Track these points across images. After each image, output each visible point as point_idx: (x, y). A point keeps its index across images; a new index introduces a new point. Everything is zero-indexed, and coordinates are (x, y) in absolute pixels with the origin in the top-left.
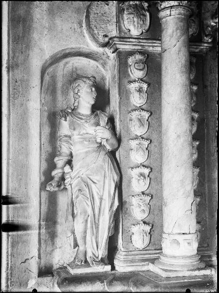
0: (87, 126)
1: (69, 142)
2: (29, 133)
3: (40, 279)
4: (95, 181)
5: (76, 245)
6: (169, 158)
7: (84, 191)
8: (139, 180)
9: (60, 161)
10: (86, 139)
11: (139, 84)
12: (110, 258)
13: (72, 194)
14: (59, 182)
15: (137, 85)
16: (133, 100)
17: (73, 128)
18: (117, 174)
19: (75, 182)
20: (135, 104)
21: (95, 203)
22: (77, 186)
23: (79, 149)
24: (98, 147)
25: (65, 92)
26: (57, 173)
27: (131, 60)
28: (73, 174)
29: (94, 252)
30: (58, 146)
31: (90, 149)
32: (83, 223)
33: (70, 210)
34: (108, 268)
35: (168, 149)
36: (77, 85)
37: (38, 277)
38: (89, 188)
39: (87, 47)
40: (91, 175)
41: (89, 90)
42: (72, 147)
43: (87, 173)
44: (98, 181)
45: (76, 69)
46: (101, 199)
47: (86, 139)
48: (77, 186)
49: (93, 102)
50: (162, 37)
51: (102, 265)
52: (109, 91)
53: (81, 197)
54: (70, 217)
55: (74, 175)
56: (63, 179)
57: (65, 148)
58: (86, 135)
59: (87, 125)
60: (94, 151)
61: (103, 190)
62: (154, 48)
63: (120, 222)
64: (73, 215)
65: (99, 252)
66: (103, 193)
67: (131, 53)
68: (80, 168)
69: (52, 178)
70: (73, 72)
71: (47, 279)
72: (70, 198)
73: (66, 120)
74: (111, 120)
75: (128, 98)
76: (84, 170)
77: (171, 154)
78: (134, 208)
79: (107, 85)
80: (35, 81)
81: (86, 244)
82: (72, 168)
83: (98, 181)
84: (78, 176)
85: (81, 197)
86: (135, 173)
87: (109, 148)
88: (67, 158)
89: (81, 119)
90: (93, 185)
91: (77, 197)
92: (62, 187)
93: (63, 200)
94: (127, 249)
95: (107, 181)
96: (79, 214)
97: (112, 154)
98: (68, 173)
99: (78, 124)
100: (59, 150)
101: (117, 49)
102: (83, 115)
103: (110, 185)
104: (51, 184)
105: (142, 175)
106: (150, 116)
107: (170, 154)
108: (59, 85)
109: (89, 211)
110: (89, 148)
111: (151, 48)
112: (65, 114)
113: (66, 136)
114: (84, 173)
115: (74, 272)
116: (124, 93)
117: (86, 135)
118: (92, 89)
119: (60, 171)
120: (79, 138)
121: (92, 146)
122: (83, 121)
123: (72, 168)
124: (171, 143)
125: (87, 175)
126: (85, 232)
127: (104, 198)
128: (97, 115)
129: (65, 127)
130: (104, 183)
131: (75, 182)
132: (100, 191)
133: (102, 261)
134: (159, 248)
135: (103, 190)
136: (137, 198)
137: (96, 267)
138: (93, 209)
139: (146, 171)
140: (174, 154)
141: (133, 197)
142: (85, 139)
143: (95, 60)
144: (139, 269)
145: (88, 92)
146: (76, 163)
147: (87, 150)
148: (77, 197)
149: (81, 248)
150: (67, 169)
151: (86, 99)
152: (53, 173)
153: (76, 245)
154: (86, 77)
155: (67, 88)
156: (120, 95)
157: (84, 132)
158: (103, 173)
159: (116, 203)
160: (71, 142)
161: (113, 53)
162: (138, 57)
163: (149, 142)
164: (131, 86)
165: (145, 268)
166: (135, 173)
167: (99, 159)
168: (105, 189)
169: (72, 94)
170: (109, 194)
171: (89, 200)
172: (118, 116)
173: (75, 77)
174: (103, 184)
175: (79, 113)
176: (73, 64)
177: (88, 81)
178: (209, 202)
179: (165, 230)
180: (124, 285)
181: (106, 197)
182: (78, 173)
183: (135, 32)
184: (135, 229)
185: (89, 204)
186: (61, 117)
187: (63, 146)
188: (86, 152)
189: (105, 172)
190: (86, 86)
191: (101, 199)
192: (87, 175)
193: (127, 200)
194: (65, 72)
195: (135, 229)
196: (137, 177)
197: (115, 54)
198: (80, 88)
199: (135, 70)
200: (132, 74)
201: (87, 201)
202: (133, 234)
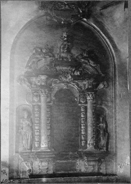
15: (36, 112)
34: (30, 151)
50: (109, 120)
62: (39, 104)
64: (23, 140)
67: (35, 105)
71: (17, 154)
74: (31, 120)
87: (30, 125)
97: (32, 127)
105: (37, 131)
116: (34, 114)
131: (23, 133)
133: (29, 150)
139: (38, 130)
150: (22, 130)
162: (37, 106)
168: (29, 134)
178: (98, 32)
181: (30, 136)
183: (36, 101)
184: (36, 143)
195: (36, 143)
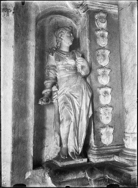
0: (68, 60)
1: (55, 70)
2: (27, 63)
3: (34, 171)
4: (76, 97)
5: (61, 144)
6: (129, 79)
7: (68, 103)
8: (104, 96)
9: (48, 84)
10: (66, 67)
11: (103, 32)
12: (85, 153)
13: (58, 107)
14: (47, 98)
16: (99, 42)
17: (58, 60)
18: (91, 92)
19: (60, 98)
20: (100, 45)
21: (76, 112)
22: (63, 100)
23: (62, 75)
24: (75, 73)
25: (51, 37)
26: (46, 92)
27: (96, 16)
28: (59, 92)
29: (76, 148)
30: (46, 73)
31: (71, 75)
32: (67, 127)
33: (57, 118)
34: (85, 160)
35: (128, 74)
36: (60, 31)
37: (33, 170)
38: (72, 102)
39: (66, 8)
40: (72, 92)
41: (69, 35)
42: (57, 74)
43: (70, 91)
44: (78, 96)
45: (58, 22)
46: (80, 110)
47: (66, 67)
48: (63, 100)
49: (71, 44)
51: (81, 158)
52: (79, 39)
53: (66, 108)
54: (57, 123)
55: (60, 92)
56: (51, 95)
57: (52, 75)
58: (67, 65)
59: (67, 58)
60: (73, 76)
61: (82, 103)
63: (92, 126)
65: (79, 148)
66: (81, 105)
68: (65, 87)
69: (43, 96)
70: (55, 25)
72: (57, 109)
73: (53, 55)
75: (96, 41)
76: (67, 89)
77: (130, 77)
78: (102, 116)
79: (78, 34)
80: (32, 27)
81: (67, 143)
82: (58, 87)
83: (78, 96)
84: (63, 93)
85: (66, 108)
86: (101, 91)
87: (83, 73)
88: (53, 81)
89: (65, 54)
90: (74, 99)
91: (63, 108)
92: (50, 102)
93: (50, 113)
94: (98, 146)
95: (84, 97)
96: (65, 120)
98: (55, 91)
99: (62, 58)
100: (47, 76)
101: (88, 8)
102: (64, 52)
103: (86, 99)
104: (42, 100)
106: (110, 53)
107: (129, 77)
108: (47, 33)
109: (73, 118)
110: (69, 74)
111: (109, 10)
112: (52, 51)
113: (53, 66)
114: (67, 91)
115: (60, 164)
116: (93, 38)
117: (67, 65)
118: (70, 35)
119: (49, 90)
120: (63, 67)
121: (72, 72)
122: (65, 56)
123: (58, 87)
124: (129, 69)
125: (70, 92)
126: (68, 134)
127: (82, 108)
128: (73, 53)
129: (52, 60)
130: (82, 97)
131: (60, 98)
132: (79, 104)
134: (121, 143)
135: (82, 103)
136: (104, 109)
137: (77, 160)
138: (75, 118)
140: (132, 77)
141: (101, 109)
142: (66, 68)
143: (70, 18)
144: (108, 160)
145: (67, 36)
146: (59, 83)
147: (68, 75)
148: (63, 108)
149: (64, 146)
151: (66, 43)
152: (44, 92)
153: (61, 144)
154: (67, 27)
155: (52, 35)
156: (90, 38)
157: (66, 63)
158: (81, 91)
159: (91, 113)
160: (57, 70)
161: (84, 12)
163: (110, 71)
164: (98, 33)
165: (112, 159)
166: (101, 91)
167: (78, 81)
169: (55, 39)
170: (86, 106)
171: (72, 110)
172: (88, 53)
173: (57, 27)
174: (81, 99)
175: (62, 51)
176: (55, 19)
177: (68, 29)
179: (127, 131)
180: (101, 173)
181: (84, 108)
182: (63, 91)
185: (73, 113)
186: (49, 53)
187: (50, 73)
188: (68, 77)
189: (82, 90)
190: (67, 32)
191: (80, 110)
192: (70, 92)
193: (97, 110)
194: (50, 24)
195: (103, 131)
196: (103, 94)
197: (85, 13)
198: (62, 34)
199: (100, 23)
200: (98, 25)
201: (70, 111)
202: (101, 134)
